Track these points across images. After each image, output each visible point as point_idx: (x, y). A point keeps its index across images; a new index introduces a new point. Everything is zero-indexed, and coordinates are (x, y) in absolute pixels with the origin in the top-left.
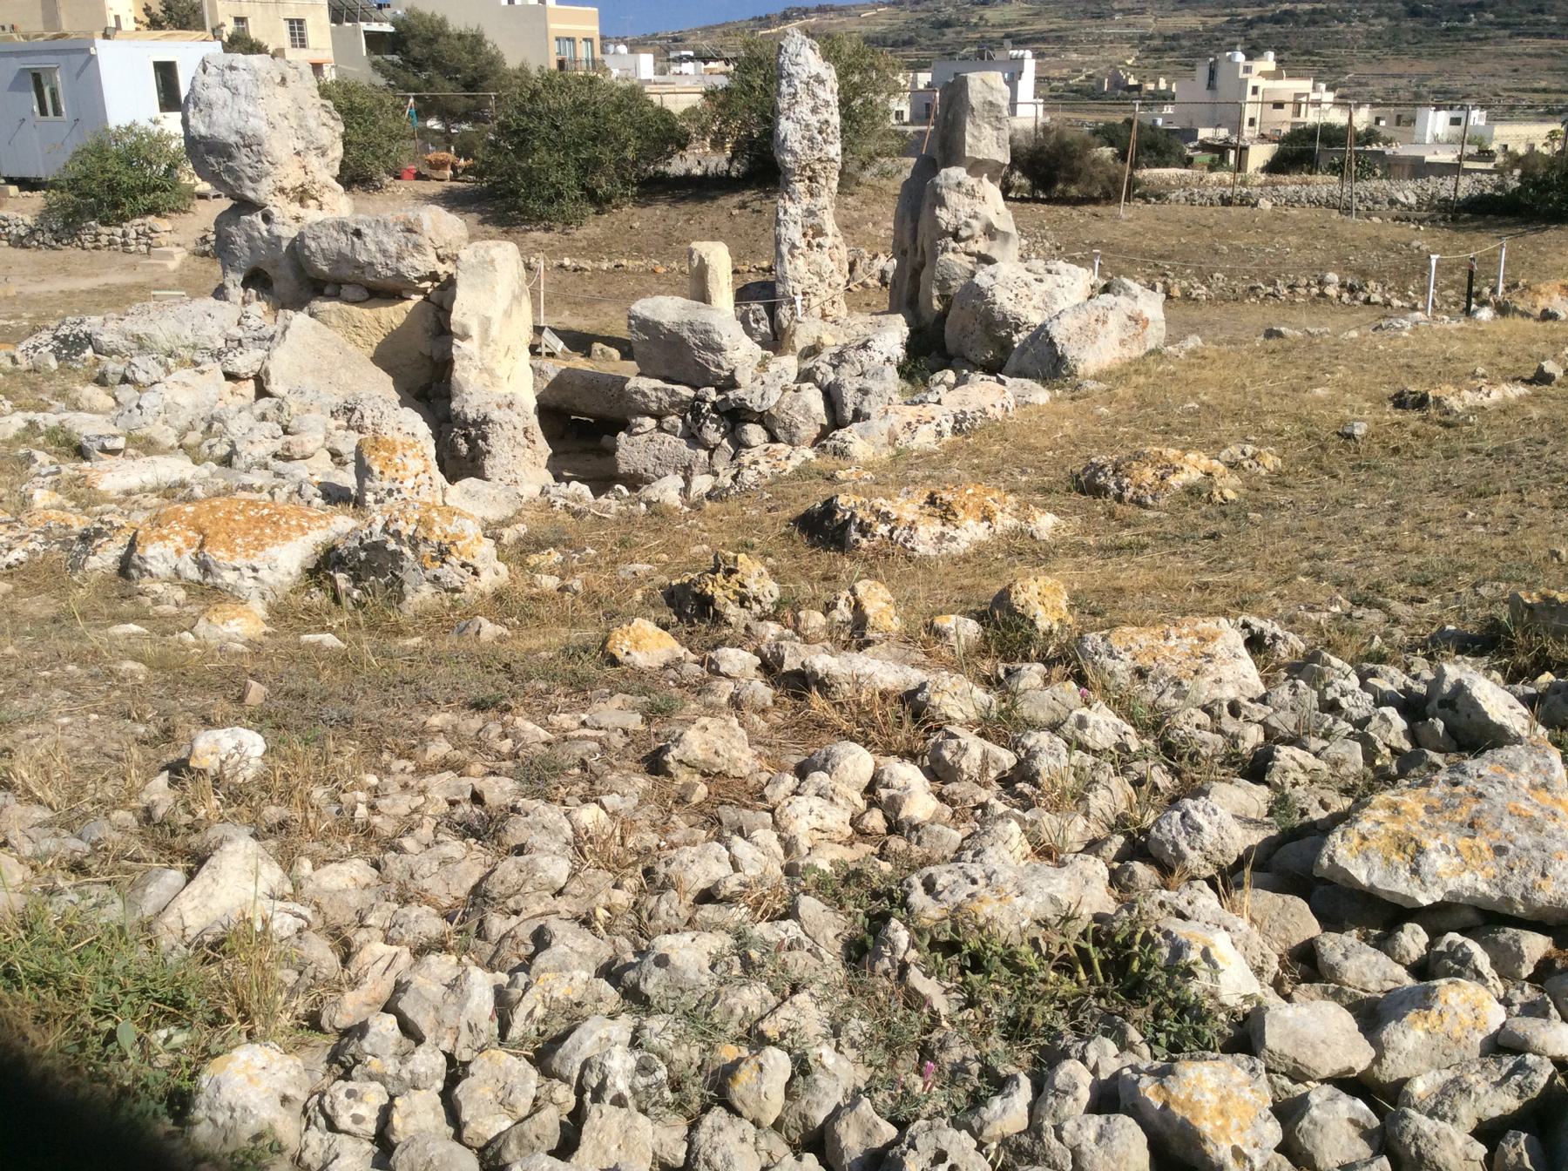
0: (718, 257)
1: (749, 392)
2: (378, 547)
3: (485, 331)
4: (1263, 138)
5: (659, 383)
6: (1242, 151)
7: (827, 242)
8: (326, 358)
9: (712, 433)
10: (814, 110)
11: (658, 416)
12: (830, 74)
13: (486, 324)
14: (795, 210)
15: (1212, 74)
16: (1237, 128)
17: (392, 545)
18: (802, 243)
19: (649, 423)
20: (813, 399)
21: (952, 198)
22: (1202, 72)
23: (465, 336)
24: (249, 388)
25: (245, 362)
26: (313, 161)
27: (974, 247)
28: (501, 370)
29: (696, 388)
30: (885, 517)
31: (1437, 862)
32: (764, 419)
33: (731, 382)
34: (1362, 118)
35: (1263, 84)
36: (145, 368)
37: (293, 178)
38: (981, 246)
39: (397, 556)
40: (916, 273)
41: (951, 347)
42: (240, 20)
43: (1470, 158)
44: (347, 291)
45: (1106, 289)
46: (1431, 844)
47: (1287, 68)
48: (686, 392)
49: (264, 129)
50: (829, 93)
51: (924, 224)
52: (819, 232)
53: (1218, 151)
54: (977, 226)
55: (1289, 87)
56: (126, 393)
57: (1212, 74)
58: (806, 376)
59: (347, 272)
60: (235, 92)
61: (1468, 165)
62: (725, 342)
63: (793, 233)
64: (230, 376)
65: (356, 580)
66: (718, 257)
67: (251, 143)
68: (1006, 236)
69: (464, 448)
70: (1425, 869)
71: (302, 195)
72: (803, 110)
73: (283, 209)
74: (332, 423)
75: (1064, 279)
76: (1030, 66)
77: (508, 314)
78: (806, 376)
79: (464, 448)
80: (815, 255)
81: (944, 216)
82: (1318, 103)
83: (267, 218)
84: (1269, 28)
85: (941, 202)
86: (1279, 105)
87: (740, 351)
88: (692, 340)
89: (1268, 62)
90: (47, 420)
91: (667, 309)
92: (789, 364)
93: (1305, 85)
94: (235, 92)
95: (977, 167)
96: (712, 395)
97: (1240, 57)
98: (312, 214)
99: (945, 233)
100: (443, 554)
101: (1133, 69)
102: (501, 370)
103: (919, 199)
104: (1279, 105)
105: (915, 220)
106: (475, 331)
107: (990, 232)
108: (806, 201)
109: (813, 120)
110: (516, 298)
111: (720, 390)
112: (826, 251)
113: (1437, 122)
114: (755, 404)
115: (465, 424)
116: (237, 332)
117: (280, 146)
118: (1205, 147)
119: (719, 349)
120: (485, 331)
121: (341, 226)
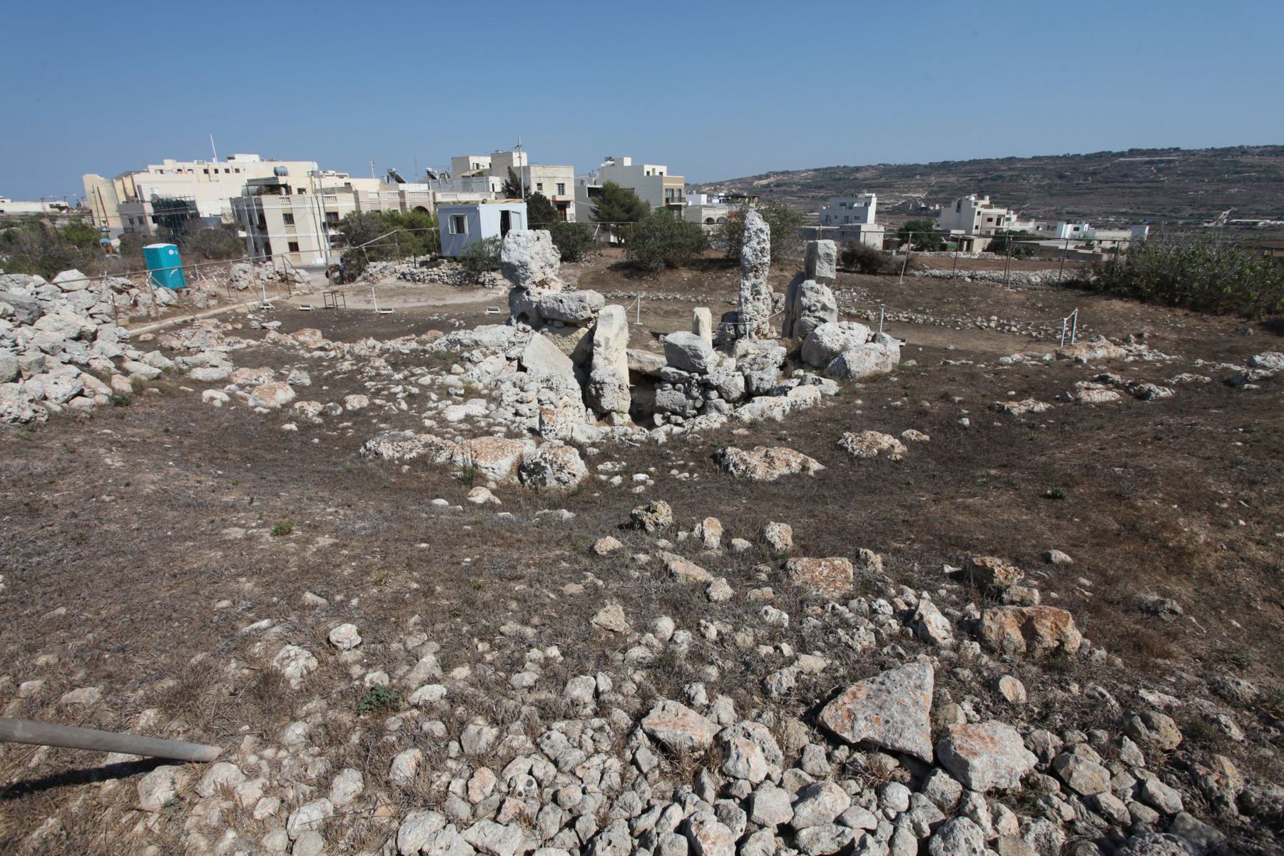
0: (705, 315)
1: (713, 377)
2: (537, 464)
3: (607, 343)
4: (981, 236)
5: (674, 370)
6: (970, 242)
7: (761, 297)
8: (547, 355)
9: (695, 392)
10: (759, 243)
11: (674, 384)
12: (766, 228)
13: (607, 340)
14: (748, 284)
15: (959, 206)
16: (969, 232)
17: (543, 464)
18: (751, 298)
19: (669, 386)
20: (740, 382)
21: (809, 293)
22: (954, 204)
23: (599, 345)
24: (515, 363)
25: (513, 353)
26: (548, 270)
27: (817, 314)
28: (615, 364)
29: (689, 372)
30: (744, 461)
31: (861, 724)
32: (717, 388)
33: (703, 372)
34: (1030, 226)
35: (983, 211)
36: (476, 354)
37: (539, 277)
38: (821, 314)
39: (544, 468)
40: (793, 322)
41: (804, 359)
42: (539, 185)
43: (1082, 248)
44: (556, 323)
45: (873, 340)
46: (860, 716)
47: (995, 203)
48: (685, 374)
49: (529, 259)
50: (766, 236)
51: (796, 303)
52: (758, 293)
53: (959, 241)
54: (819, 306)
55: (996, 211)
56: (468, 365)
57: (959, 206)
58: (739, 369)
59: (556, 316)
60: (519, 245)
61: (1081, 251)
62: (703, 355)
63: (747, 293)
64: (508, 359)
65: (529, 476)
66: (705, 315)
67: (524, 265)
68: (832, 310)
69: (594, 392)
70: (856, 727)
71: (542, 283)
72: (754, 243)
73: (534, 290)
74: (541, 386)
75: (854, 332)
76: (874, 201)
77: (617, 335)
78: (739, 369)
79: (594, 392)
80: (756, 303)
81: (804, 300)
82: (1008, 219)
83: (528, 294)
84: (989, 182)
85: (804, 295)
86: (990, 220)
87: (710, 357)
88: (690, 353)
89: (987, 201)
90: (440, 380)
91: (680, 338)
92: (731, 363)
93: (1004, 211)
94: (519, 245)
95: (820, 280)
96: (696, 376)
97: (973, 198)
98: (546, 292)
99: (804, 308)
100: (561, 468)
101: (924, 200)
102: (615, 364)
103: (795, 292)
104: (990, 220)
105: (794, 299)
106: (602, 343)
107: (824, 308)
108: (753, 280)
109: (758, 248)
110: (622, 329)
111: (700, 374)
112: (760, 302)
113: (1067, 230)
114: (715, 382)
115: (595, 383)
116: (513, 339)
117: (534, 266)
118: (955, 240)
119: (701, 358)
120: (607, 343)
121: (556, 299)
